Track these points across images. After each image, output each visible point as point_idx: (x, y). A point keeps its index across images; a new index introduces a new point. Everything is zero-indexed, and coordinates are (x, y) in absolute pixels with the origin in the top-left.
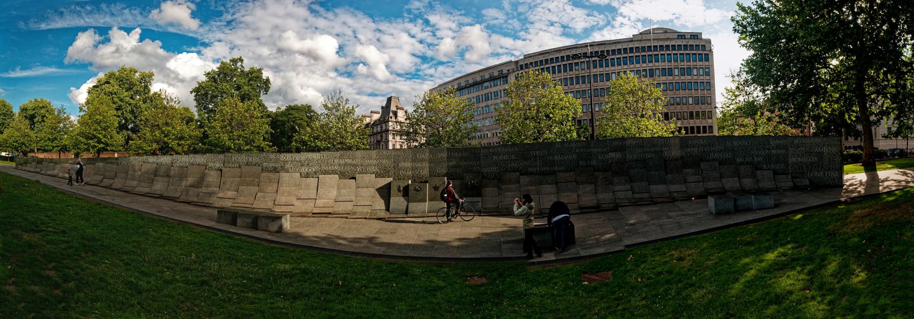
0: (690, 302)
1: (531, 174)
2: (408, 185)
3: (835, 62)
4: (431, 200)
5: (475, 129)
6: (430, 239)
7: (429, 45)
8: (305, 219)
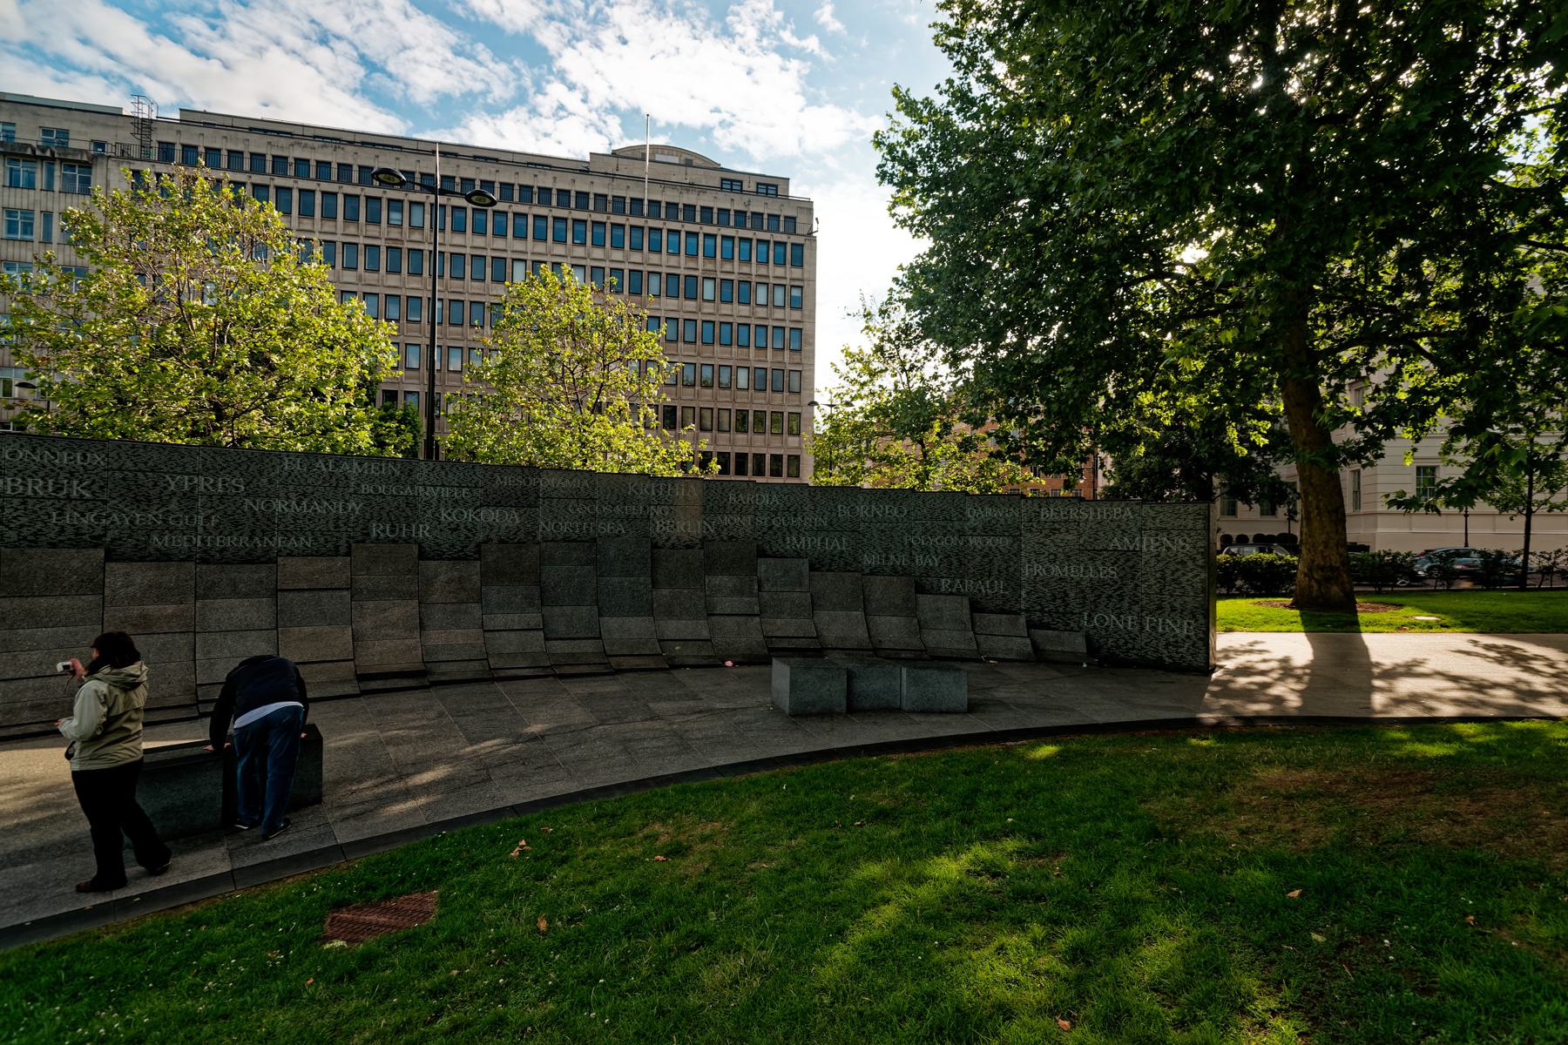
0: (693, 1000)
1: (164, 557)
3: (1193, 253)
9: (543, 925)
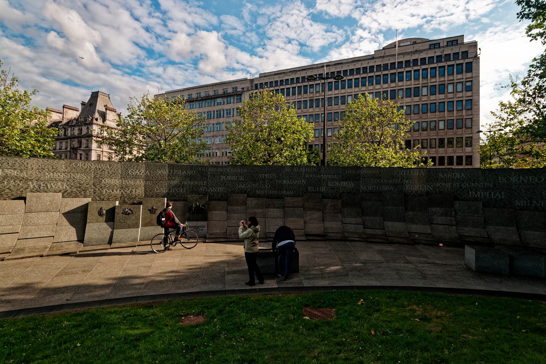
1: (259, 196)
5: (204, 146)
7: (158, 37)
9: (373, 332)
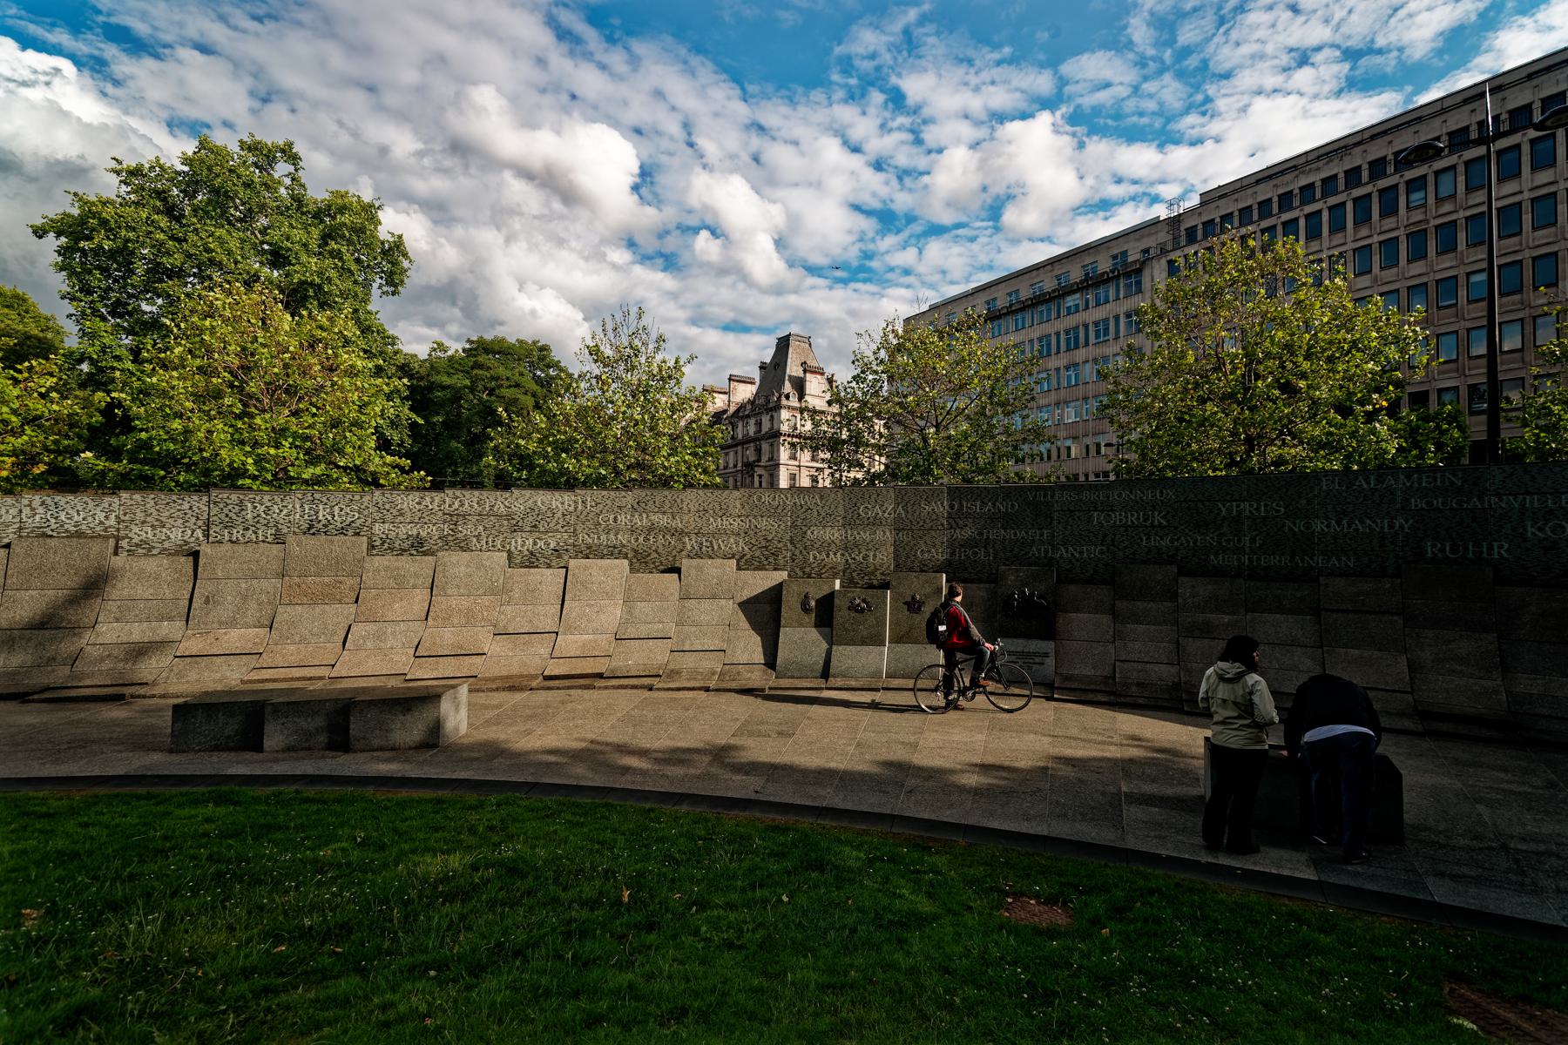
2: (831, 596)
4: (898, 639)
6: (892, 757)
7: (903, 174)
8: (519, 697)
